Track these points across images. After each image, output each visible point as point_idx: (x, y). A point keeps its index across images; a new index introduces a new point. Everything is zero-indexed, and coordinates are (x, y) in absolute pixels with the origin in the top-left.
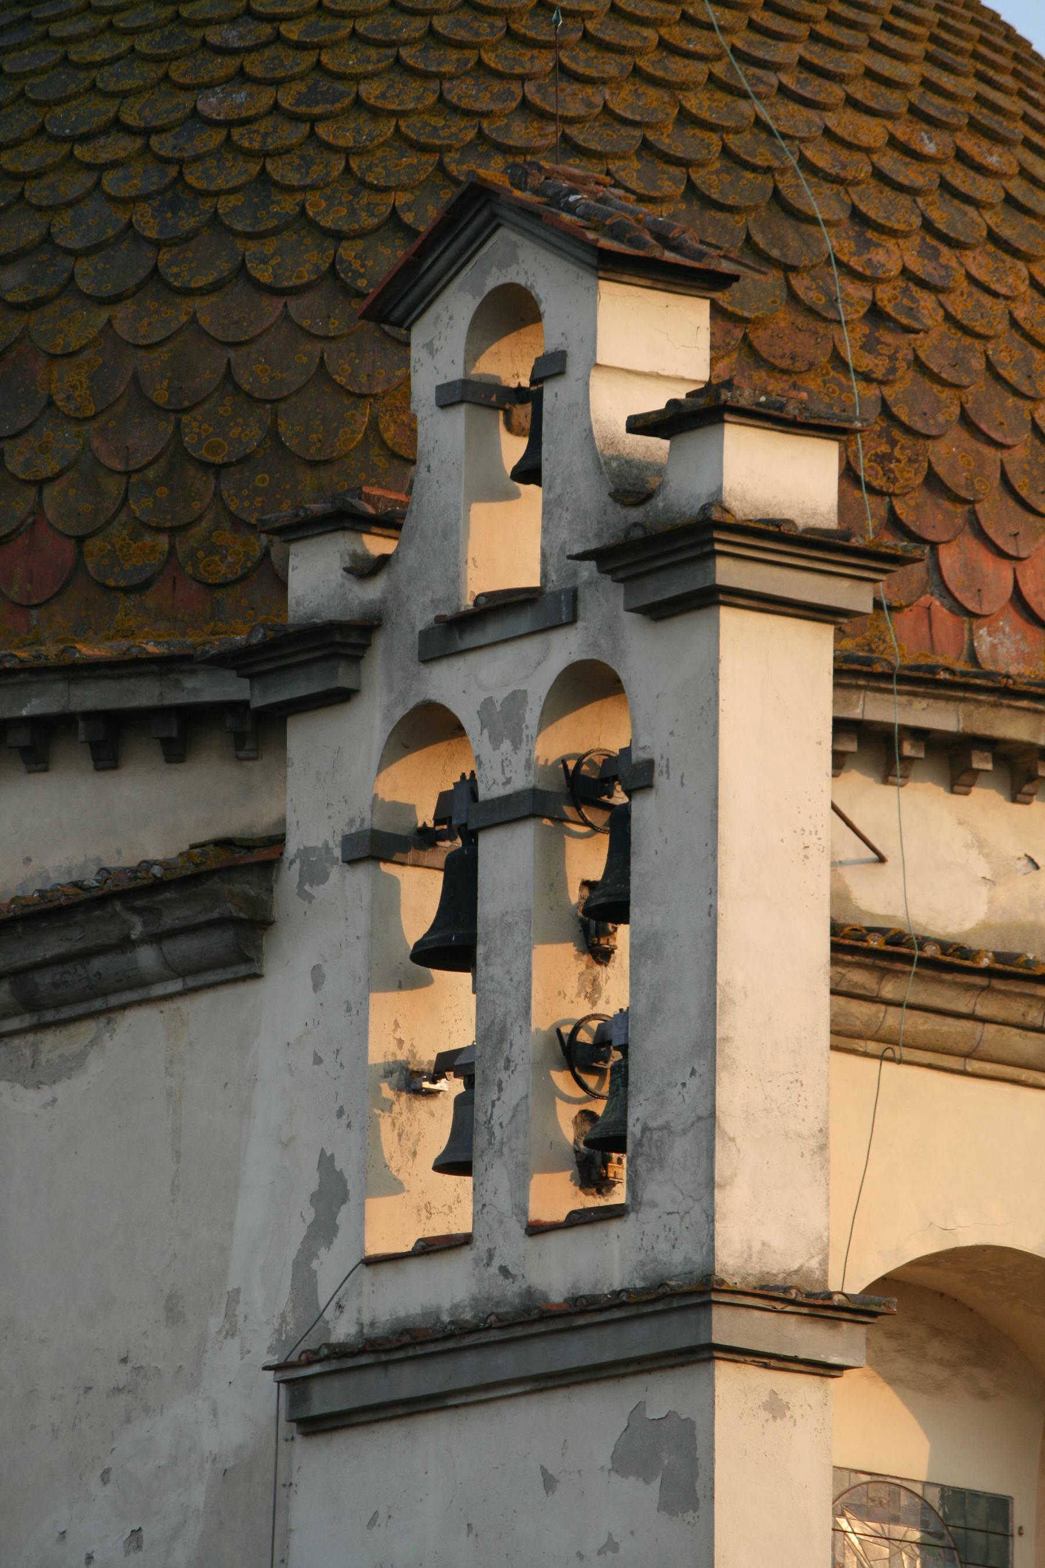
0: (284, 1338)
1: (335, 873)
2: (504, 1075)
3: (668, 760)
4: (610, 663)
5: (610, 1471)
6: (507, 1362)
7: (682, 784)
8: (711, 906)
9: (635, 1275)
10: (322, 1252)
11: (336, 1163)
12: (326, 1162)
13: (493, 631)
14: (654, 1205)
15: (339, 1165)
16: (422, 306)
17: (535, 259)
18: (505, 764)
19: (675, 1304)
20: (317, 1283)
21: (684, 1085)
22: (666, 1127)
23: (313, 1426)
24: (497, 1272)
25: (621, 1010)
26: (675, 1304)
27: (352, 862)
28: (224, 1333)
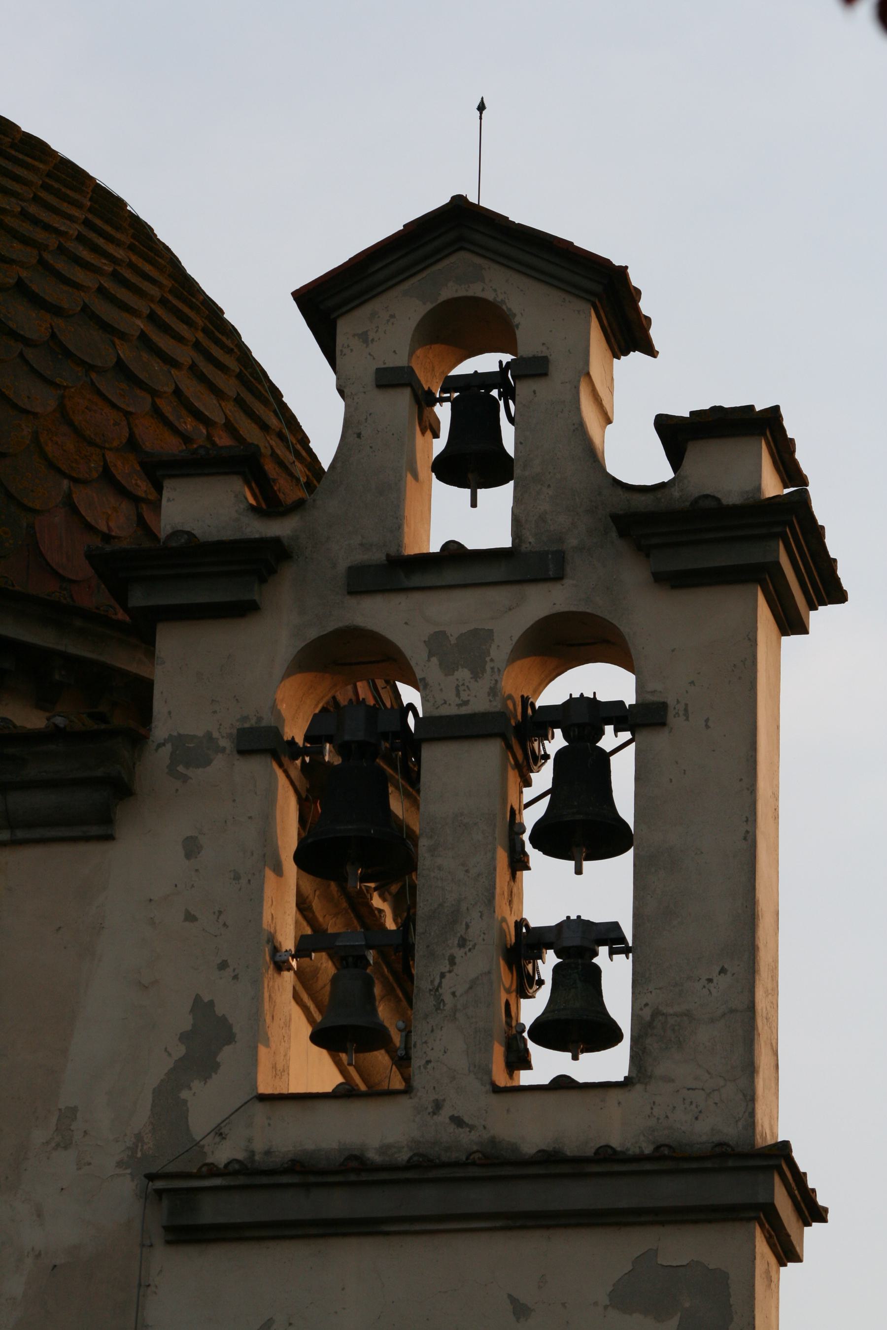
0: (139, 1155)
1: (219, 762)
2: (459, 953)
3: (686, 705)
4: (608, 617)
5: (606, 1307)
6: (482, 1198)
7: (707, 727)
8: (747, 832)
9: (642, 1138)
10: (196, 1085)
11: (216, 1009)
12: (202, 1008)
13: (451, 576)
14: (668, 1080)
15: (220, 1010)
16: (357, 302)
17: (507, 281)
18: (461, 688)
19: (730, 1163)
20: (188, 1110)
21: (710, 980)
22: (688, 1014)
23: (185, 1234)
24: (447, 1120)
25: (568, 917)
26: (730, 1163)
27: (243, 752)
28: (53, 1144)
